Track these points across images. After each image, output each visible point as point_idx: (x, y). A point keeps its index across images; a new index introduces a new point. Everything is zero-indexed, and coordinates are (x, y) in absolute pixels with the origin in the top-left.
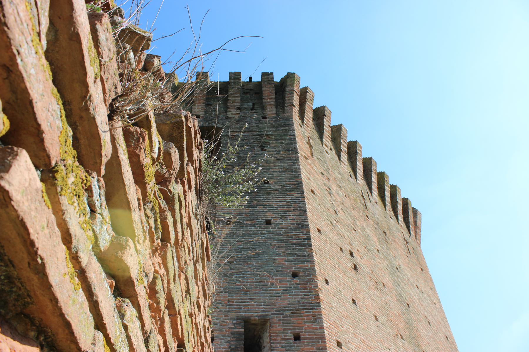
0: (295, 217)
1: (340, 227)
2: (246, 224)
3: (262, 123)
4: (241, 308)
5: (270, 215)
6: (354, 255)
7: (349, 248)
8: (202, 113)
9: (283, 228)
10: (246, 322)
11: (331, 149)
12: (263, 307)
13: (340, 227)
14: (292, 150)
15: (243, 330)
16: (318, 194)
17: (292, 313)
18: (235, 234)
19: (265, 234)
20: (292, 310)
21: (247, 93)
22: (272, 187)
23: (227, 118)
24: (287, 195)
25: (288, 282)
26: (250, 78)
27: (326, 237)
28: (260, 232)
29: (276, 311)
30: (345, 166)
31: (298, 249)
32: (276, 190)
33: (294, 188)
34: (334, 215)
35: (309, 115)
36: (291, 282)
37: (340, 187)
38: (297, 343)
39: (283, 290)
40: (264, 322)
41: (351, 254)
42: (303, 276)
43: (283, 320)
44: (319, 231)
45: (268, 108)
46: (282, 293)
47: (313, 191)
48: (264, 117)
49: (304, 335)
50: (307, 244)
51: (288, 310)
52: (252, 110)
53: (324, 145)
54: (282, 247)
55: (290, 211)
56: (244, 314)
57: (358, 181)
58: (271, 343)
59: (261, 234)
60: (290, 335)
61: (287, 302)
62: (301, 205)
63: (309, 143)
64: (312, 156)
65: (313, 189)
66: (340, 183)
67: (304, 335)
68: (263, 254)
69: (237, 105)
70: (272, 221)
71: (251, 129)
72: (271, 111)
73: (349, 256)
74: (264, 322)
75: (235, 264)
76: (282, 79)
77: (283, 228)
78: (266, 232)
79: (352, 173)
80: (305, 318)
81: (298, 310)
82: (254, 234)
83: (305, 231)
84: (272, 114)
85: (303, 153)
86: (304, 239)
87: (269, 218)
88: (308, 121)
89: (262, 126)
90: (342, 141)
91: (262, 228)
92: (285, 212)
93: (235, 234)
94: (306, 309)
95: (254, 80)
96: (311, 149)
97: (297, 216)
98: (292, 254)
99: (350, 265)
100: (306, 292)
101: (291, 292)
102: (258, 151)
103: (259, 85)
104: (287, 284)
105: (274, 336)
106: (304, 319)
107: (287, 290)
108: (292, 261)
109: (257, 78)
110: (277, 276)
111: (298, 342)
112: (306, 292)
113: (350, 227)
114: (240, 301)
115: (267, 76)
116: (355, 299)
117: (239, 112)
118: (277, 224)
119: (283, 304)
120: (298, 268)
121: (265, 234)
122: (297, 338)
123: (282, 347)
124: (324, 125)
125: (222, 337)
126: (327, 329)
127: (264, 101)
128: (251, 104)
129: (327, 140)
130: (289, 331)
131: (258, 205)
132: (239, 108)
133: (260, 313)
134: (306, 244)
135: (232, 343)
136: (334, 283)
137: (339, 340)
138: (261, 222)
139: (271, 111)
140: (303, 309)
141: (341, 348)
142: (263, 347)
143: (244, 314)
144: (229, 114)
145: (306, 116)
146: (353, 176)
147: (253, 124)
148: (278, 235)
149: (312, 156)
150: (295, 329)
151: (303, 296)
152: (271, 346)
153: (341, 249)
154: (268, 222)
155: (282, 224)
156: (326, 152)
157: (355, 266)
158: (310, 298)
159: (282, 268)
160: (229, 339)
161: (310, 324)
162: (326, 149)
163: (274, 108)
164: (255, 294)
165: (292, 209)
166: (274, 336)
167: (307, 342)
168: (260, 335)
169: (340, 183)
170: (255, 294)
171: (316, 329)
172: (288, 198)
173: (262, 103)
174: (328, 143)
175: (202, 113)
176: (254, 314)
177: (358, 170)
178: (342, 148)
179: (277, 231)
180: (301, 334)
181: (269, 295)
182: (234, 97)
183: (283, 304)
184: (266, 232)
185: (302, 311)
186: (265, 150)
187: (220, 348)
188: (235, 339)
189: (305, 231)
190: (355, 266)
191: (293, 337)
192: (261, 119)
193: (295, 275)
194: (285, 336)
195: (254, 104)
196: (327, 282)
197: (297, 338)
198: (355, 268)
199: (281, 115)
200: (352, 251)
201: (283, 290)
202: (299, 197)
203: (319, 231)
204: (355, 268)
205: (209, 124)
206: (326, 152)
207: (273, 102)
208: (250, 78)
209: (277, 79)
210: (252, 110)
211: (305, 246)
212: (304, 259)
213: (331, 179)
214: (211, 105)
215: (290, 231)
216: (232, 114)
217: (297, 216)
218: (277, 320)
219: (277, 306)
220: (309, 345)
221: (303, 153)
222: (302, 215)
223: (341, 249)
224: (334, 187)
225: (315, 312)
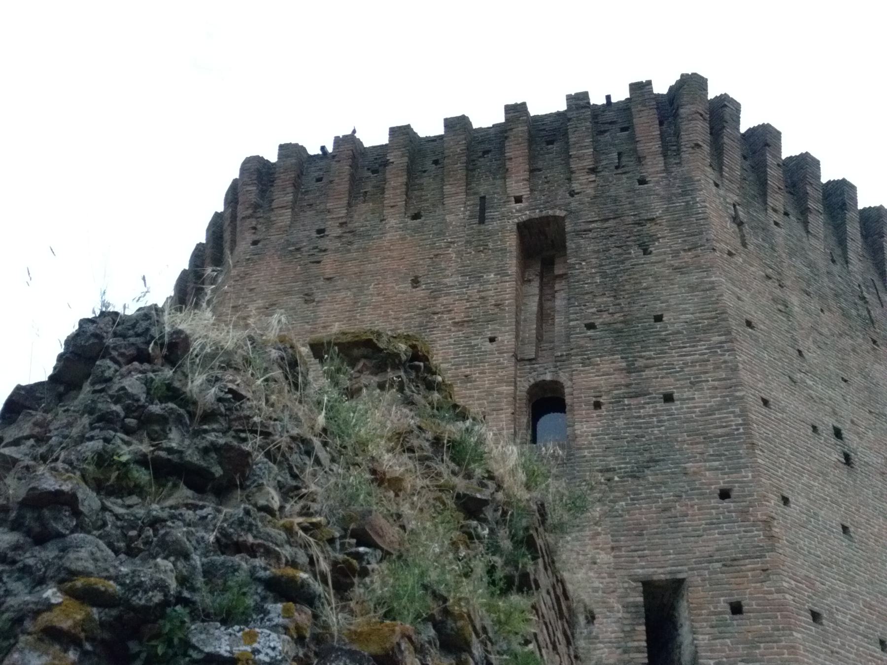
0: (716, 383)
1: (811, 383)
2: (629, 405)
3: (639, 195)
4: (634, 562)
5: (668, 384)
6: (845, 433)
7: (831, 421)
8: (524, 192)
9: (696, 407)
10: (649, 587)
11: (786, 214)
12: (672, 556)
13: (811, 383)
14: (701, 246)
15: (641, 599)
16: (762, 326)
17: (724, 565)
18: (611, 426)
19: (664, 421)
20: (724, 560)
21: (605, 131)
22: (669, 328)
23: (572, 194)
24: (700, 341)
25: (713, 508)
26: (608, 98)
27: (783, 411)
28: (655, 419)
29: (696, 563)
30: (818, 245)
31: (728, 445)
32: (678, 332)
33: (712, 325)
34: (797, 362)
35: (733, 159)
36: (718, 508)
37: (808, 294)
38: (738, 619)
39: (706, 524)
40: (676, 586)
41: (838, 433)
42: (738, 496)
43: (710, 579)
44: (766, 402)
45: (649, 161)
46: (705, 530)
47: (749, 324)
48: (642, 182)
49: (748, 605)
50: (744, 434)
51: (717, 561)
52: (617, 168)
53: (770, 211)
54: (697, 443)
55: (706, 373)
56: (640, 571)
57: (851, 267)
58: (693, 621)
59: (659, 421)
60: (723, 605)
61: (713, 547)
62: (726, 357)
63: (735, 219)
64: (744, 245)
65: (749, 317)
66: (809, 285)
67: (748, 605)
68: (663, 460)
69: (588, 163)
70: (676, 395)
71: (619, 212)
72: (654, 166)
73: (833, 440)
74: (676, 586)
75: (617, 482)
76: (671, 88)
77: (696, 407)
78: (666, 418)
79: (838, 251)
80: (749, 574)
81: (735, 560)
82: (644, 423)
83: (737, 410)
84: (657, 172)
85: (723, 245)
86: (736, 425)
87: (669, 389)
88: (731, 169)
89: (639, 201)
90: (808, 188)
91: (657, 411)
92: (697, 375)
93: (611, 426)
94: (750, 557)
95: (614, 100)
96: (741, 230)
97: (720, 380)
98: (717, 455)
99: (836, 456)
100: (746, 526)
101: (720, 528)
102: (637, 257)
103: (625, 107)
104: (711, 514)
105: (695, 609)
106: (747, 576)
107: (712, 524)
108: (717, 469)
109: (621, 94)
110: (693, 499)
111: (738, 617)
112: (746, 526)
113: (833, 376)
114: (632, 547)
115: (640, 89)
116: (847, 524)
117: (592, 177)
118: (684, 400)
119: (707, 549)
120: (728, 482)
121: (664, 421)
122: (736, 609)
123: (712, 627)
124: (766, 166)
125: (608, 614)
126: (791, 592)
127: (640, 147)
128: (615, 155)
129: (778, 200)
130: (722, 599)
131: (647, 367)
132: (593, 171)
133: (669, 569)
134: (740, 434)
135: (626, 622)
136: (801, 500)
137: (816, 609)
138: (655, 398)
139: (654, 166)
140: (744, 558)
141: (821, 624)
142: (679, 625)
143: (640, 571)
144: (576, 186)
145: (726, 161)
146: (840, 261)
147: (623, 199)
148: (688, 421)
149: (744, 245)
150: (732, 595)
151: (743, 533)
152: (692, 627)
153: (815, 428)
154: (668, 398)
155: (693, 399)
156: (776, 224)
157: (847, 457)
158: (756, 536)
159: (702, 484)
160: (620, 615)
161: (759, 585)
162: (775, 217)
163: (661, 159)
164: (657, 533)
165: (710, 367)
166: (695, 609)
167: (755, 618)
168: (672, 604)
169: (809, 285)
170: (657, 533)
171: (770, 593)
172: (702, 347)
173: (635, 150)
174: (777, 203)
175: (524, 192)
176: (660, 574)
177: (850, 244)
178: (811, 205)
179: (685, 413)
180: (743, 603)
181: (680, 534)
182: (581, 148)
183: (707, 549)
184: (666, 418)
185: (742, 562)
186: (650, 253)
187: (606, 632)
188: (629, 615)
189: (737, 410)
190: (847, 457)
191: (729, 610)
192: (637, 186)
193: (725, 494)
194: (716, 607)
195: (620, 154)
196: (786, 501)
197: (736, 609)
198: (848, 459)
199: (675, 170)
200: (839, 426)
201: (706, 524)
202: (721, 343)
203: (766, 402)
204: (848, 459)
205: (541, 211)
206: (776, 224)
207: (655, 146)
208: (608, 98)
209: (661, 87)
210: (617, 168)
211: (739, 439)
212: (739, 463)
213: (788, 283)
214: (540, 170)
215: (711, 412)
216: (581, 184)
217: (720, 380)
218: (699, 579)
219: (698, 554)
220: (759, 623)
221: (723, 245)
222: (729, 379)
223: (815, 428)
224: (794, 300)
225: (767, 562)
